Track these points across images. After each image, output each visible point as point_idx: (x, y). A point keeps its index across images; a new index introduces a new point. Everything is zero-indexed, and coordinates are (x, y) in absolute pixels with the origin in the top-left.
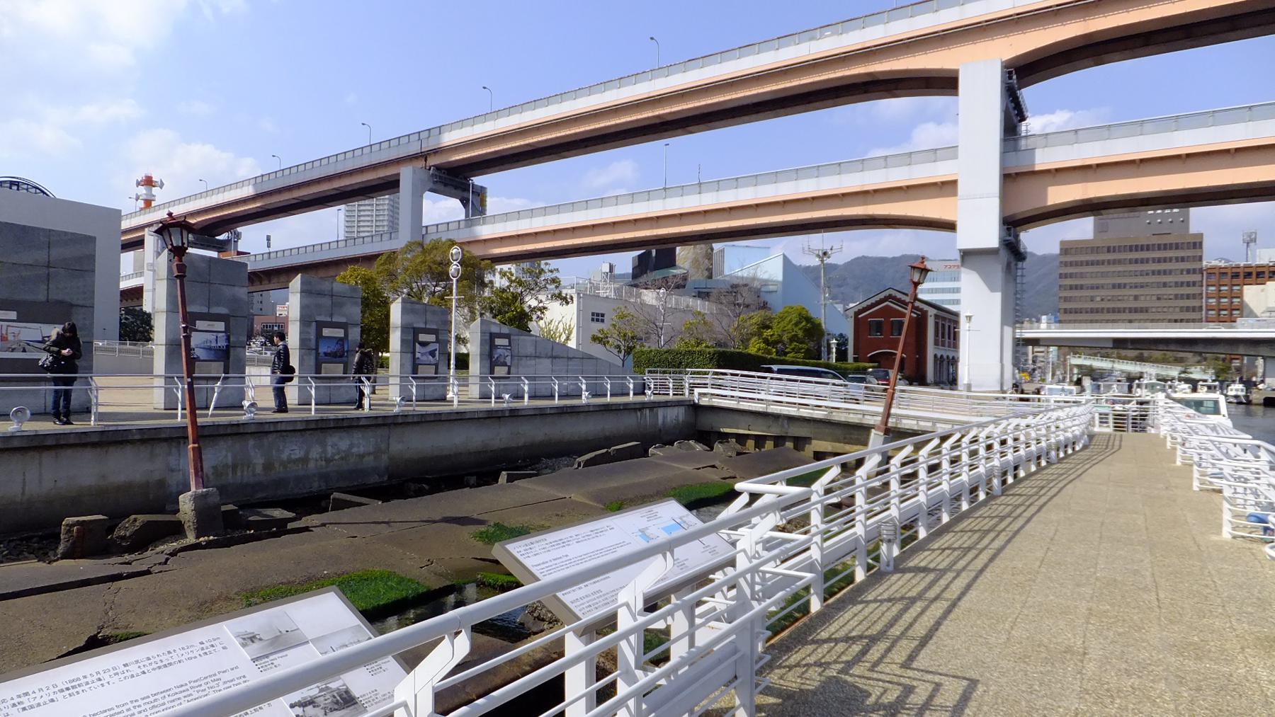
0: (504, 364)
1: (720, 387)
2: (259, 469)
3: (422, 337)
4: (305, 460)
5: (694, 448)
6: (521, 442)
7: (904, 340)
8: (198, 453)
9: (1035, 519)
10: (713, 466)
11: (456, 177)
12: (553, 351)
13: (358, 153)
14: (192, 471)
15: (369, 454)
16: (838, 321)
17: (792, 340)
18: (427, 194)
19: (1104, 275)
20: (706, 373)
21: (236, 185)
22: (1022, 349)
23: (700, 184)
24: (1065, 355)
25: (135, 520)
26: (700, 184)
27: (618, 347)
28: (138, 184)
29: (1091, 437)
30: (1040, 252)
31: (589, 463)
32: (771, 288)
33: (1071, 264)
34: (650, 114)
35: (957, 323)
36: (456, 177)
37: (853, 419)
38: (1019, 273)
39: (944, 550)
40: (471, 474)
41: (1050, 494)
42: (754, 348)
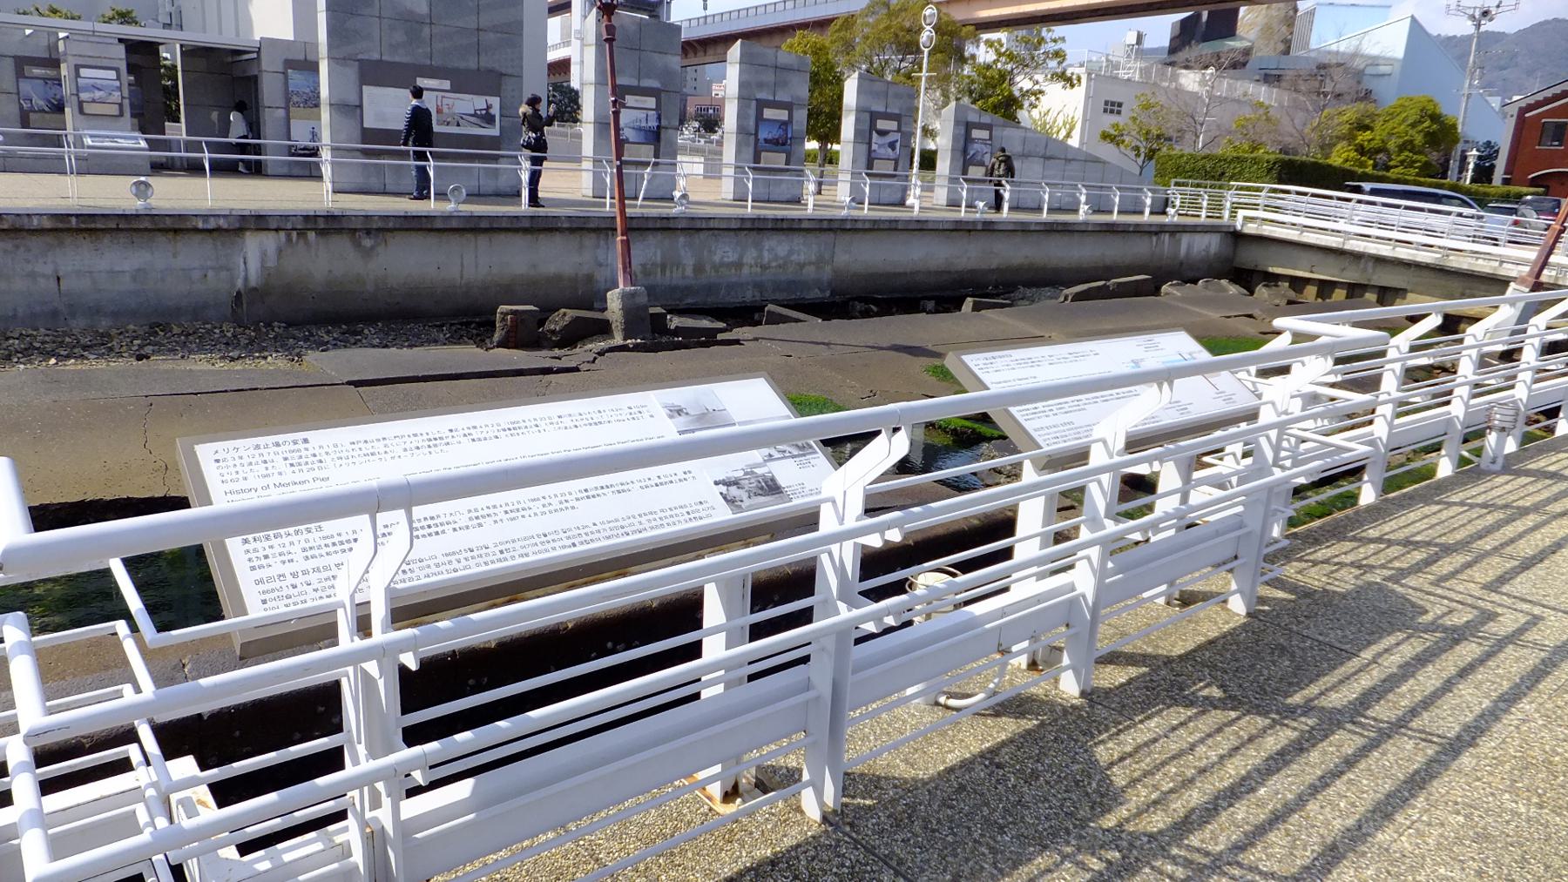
0: (981, 164)
2: (689, 272)
3: (882, 124)
4: (739, 265)
5: (1224, 290)
6: (995, 263)
8: (627, 245)
10: (1250, 316)
12: (1050, 151)
15: (810, 263)
16: (1486, 120)
20: (1259, 190)
27: (1137, 149)
31: (1078, 297)
32: (1383, 69)
40: (929, 299)
42: (1339, 157)
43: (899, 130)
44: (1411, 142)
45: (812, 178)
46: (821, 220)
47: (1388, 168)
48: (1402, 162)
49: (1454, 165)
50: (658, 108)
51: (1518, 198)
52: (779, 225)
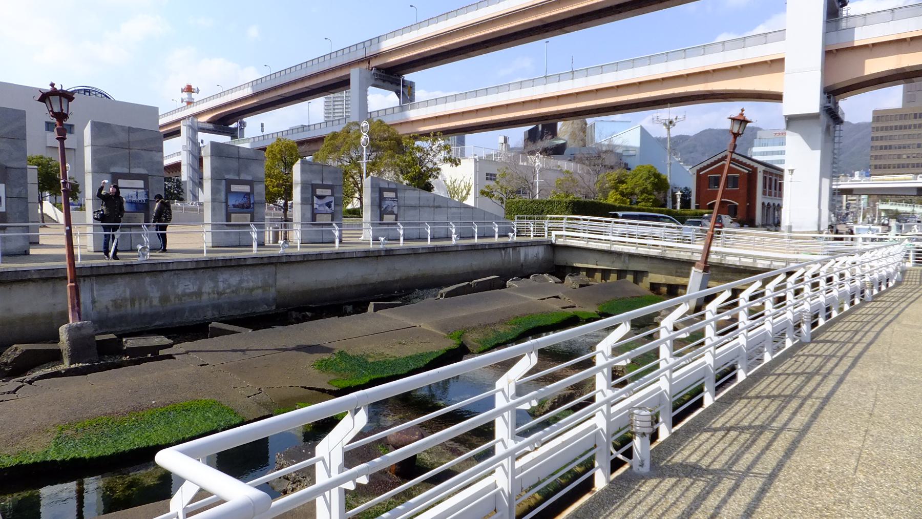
0: (392, 213)
1: (574, 230)
2: (156, 302)
3: (319, 192)
4: (199, 294)
5: (547, 281)
6: (398, 276)
7: (739, 191)
8: (76, 291)
9: (848, 378)
10: (557, 297)
11: (392, 74)
12: (451, 206)
13: (321, 60)
14: (70, 306)
15: (258, 288)
16: (682, 177)
17: (642, 192)
18: (371, 89)
19: (910, 137)
20: (562, 219)
21: (240, 87)
22: (836, 198)
23: (573, 72)
24: (874, 202)
25: (16, 349)
26: (573, 72)
27: (501, 199)
28: (183, 91)
29: (904, 272)
30: (855, 121)
31: (449, 295)
32: (631, 153)
33: (882, 129)
34: (534, 19)
35: (782, 177)
36: (392, 74)
37: (684, 256)
38: (837, 133)
39: (729, 430)
40: (349, 304)
41: (866, 340)
42: (612, 199)
43: (332, 195)
44: (646, 188)
45: (337, 228)
46: (304, 255)
47: (637, 203)
48: (643, 199)
49: (669, 200)
50: (146, 187)
51: (702, 214)
52: (154, 268)
